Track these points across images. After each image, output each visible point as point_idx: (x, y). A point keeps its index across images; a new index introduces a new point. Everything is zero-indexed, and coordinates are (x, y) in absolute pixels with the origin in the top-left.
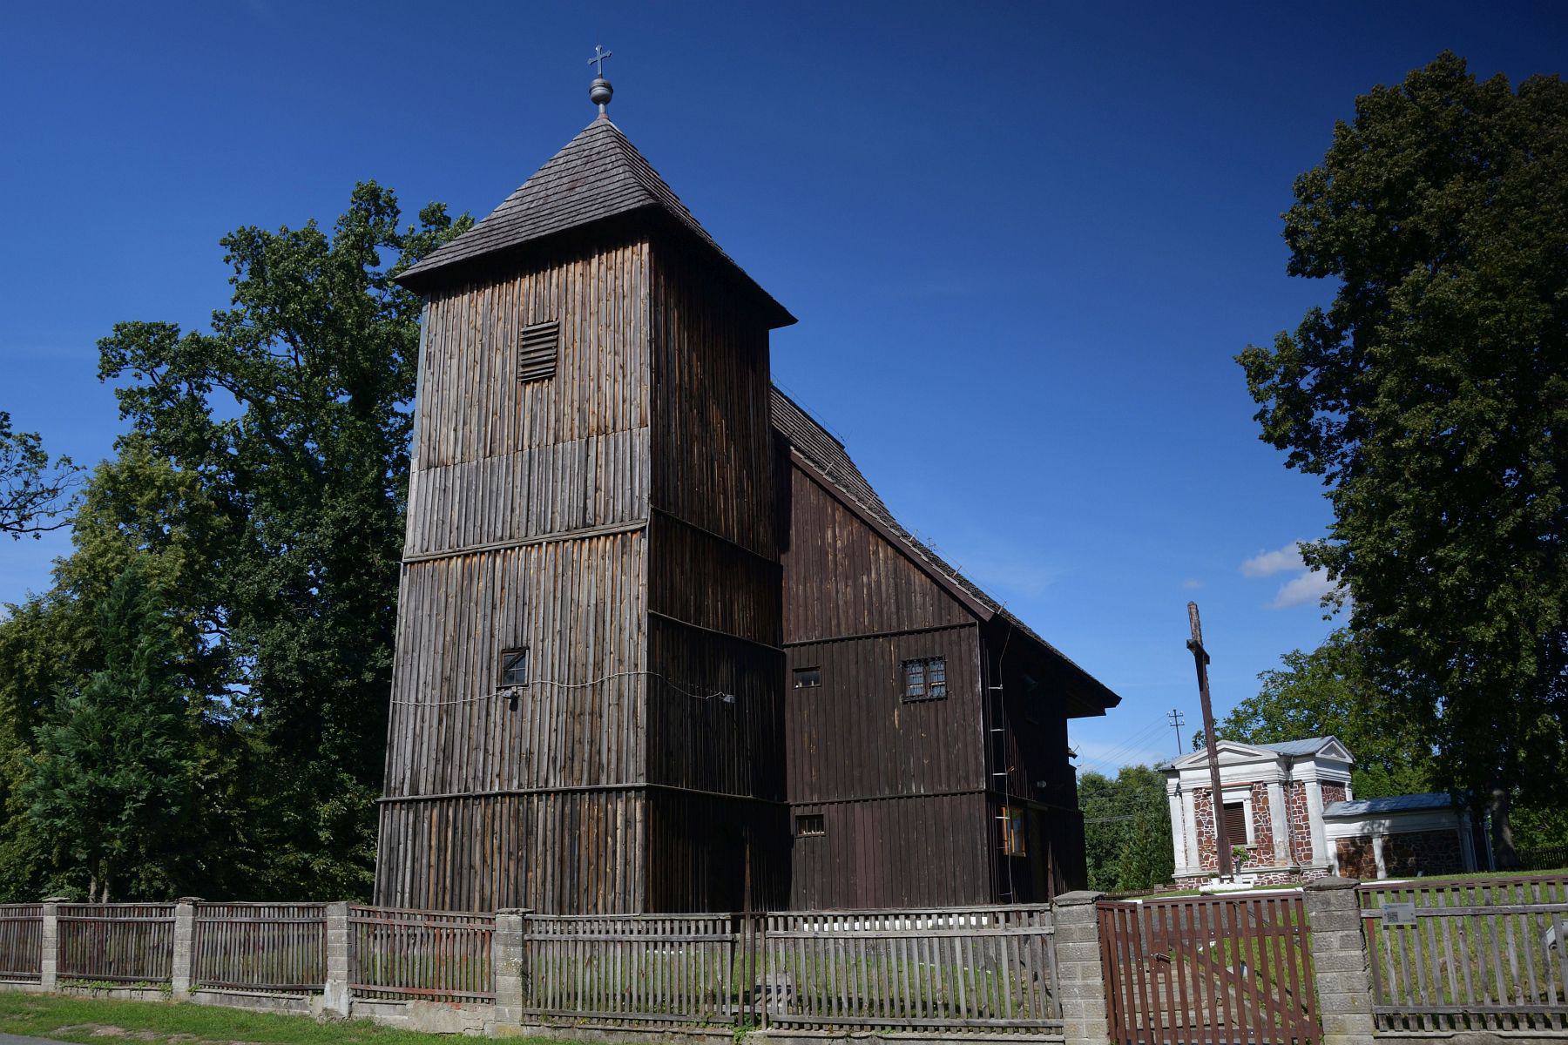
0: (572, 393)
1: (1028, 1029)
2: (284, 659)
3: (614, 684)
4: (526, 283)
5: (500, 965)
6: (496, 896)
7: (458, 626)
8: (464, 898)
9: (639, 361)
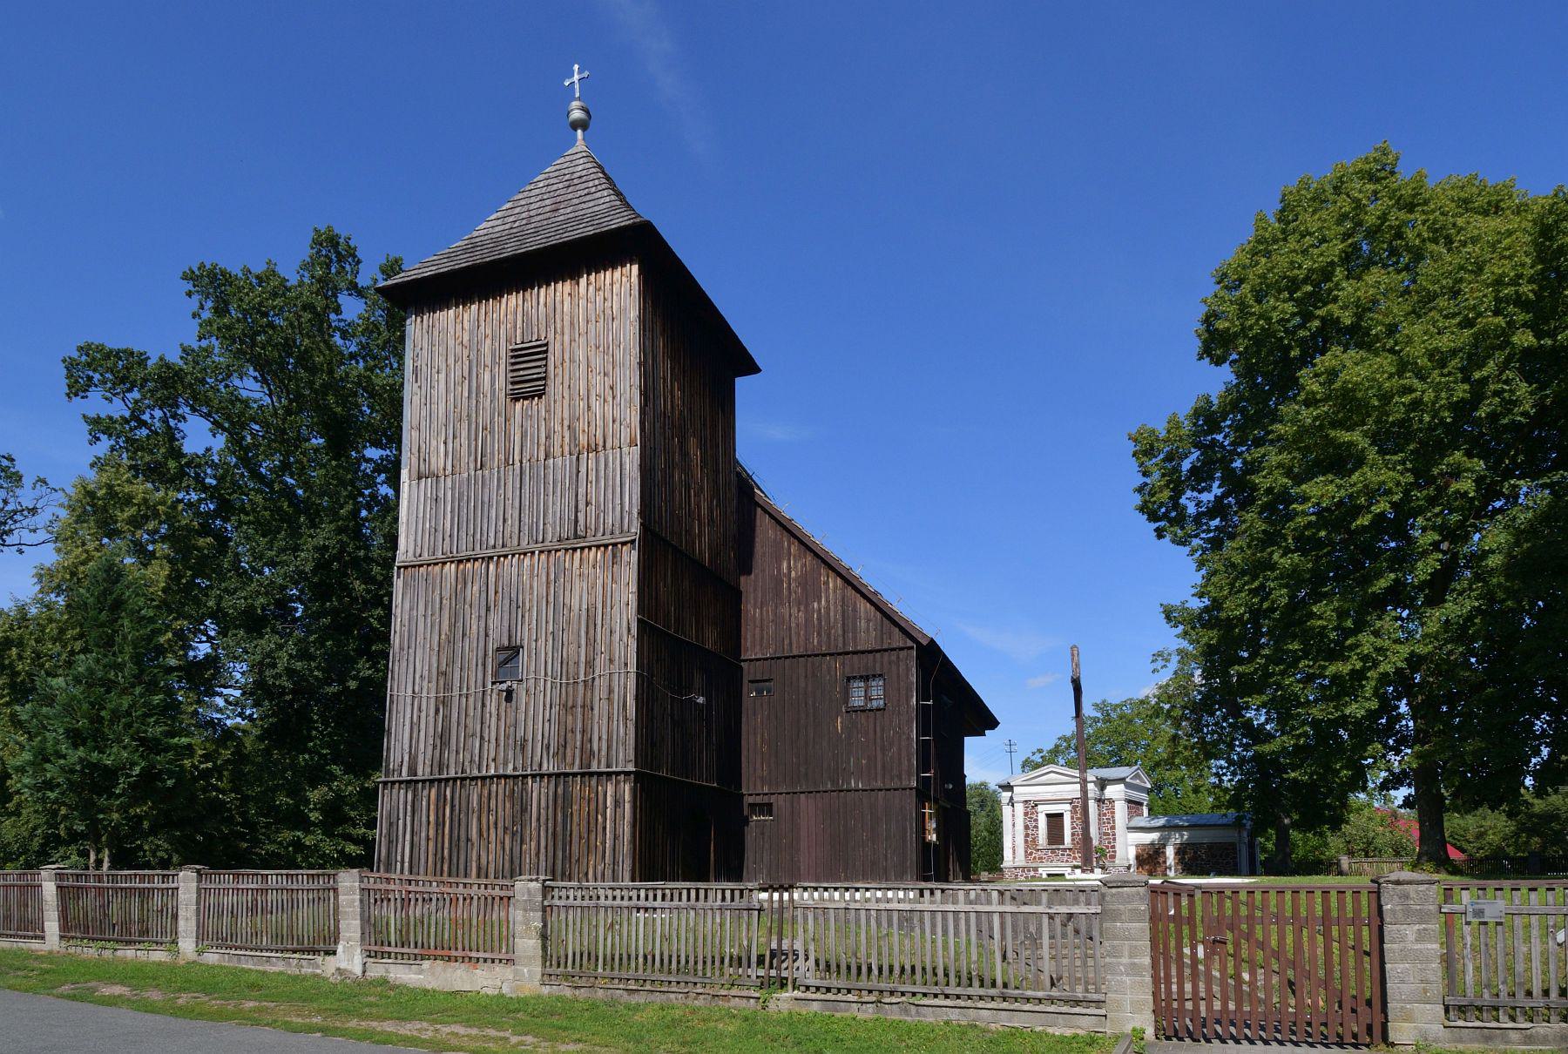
0: (562, 411)
1: (1066, 1002)
2: (274, 666)
3: (604, 682)
4: (512, 301)
5: (519, 928)
6: (492, 867)
7: (453, 626)
8: (462, 867)
9: (629, 382)
